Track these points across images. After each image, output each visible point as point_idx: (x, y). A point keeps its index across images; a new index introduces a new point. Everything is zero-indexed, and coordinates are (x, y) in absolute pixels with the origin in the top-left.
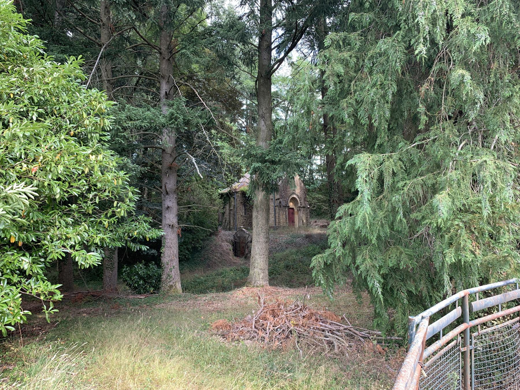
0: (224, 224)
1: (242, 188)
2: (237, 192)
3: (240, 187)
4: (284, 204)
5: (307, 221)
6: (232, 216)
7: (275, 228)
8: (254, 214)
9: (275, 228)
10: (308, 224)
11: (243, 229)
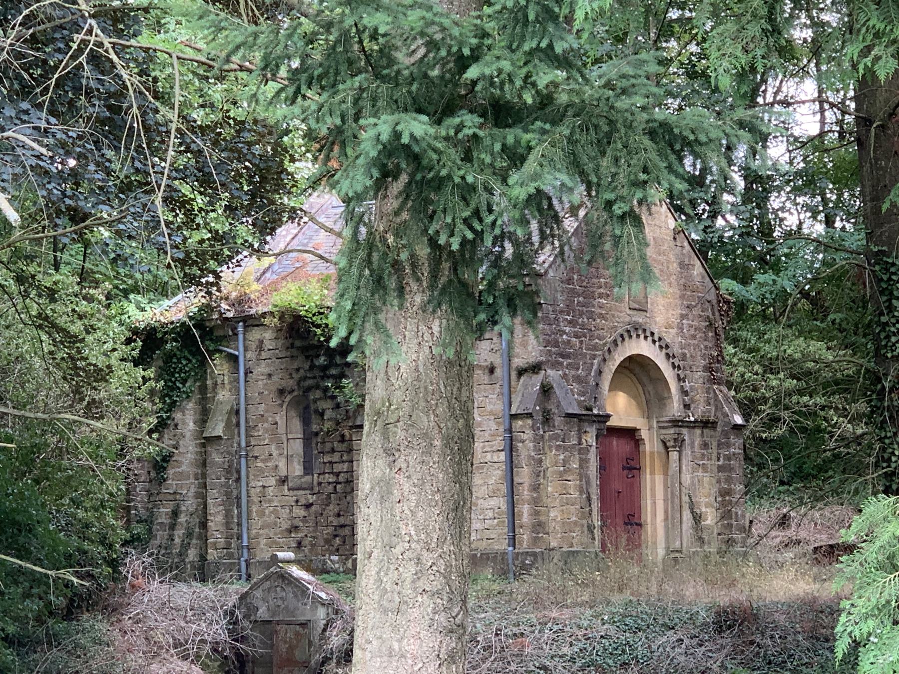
0: (161, 536)
1: (289, 295)
2: (251, 322)
3: (274, 287)
4: (569, 399)
5: (726, 514)
6: (216, 479)
7: (512, 565)
8: (369, 469)
9: (512, 565)
10: (733, 536)
11: (296, 572)
